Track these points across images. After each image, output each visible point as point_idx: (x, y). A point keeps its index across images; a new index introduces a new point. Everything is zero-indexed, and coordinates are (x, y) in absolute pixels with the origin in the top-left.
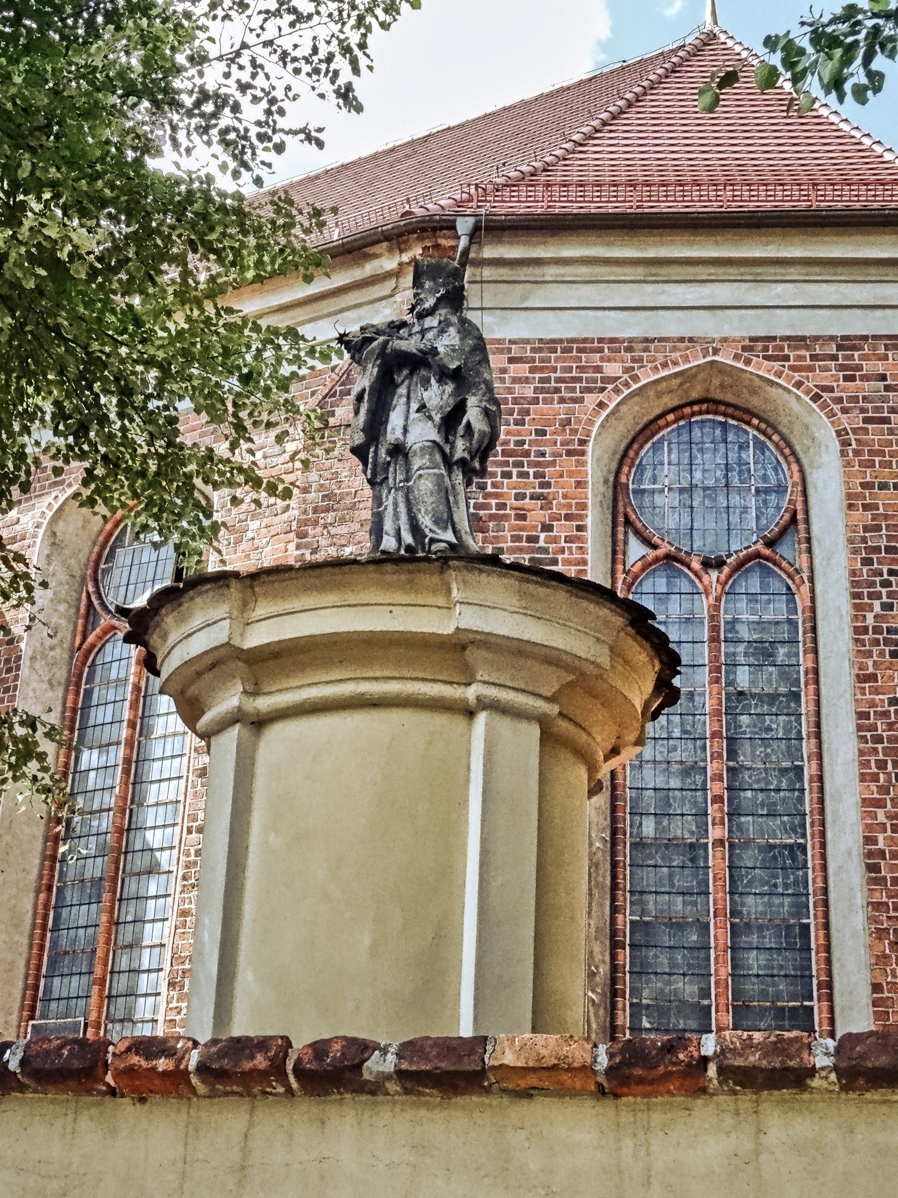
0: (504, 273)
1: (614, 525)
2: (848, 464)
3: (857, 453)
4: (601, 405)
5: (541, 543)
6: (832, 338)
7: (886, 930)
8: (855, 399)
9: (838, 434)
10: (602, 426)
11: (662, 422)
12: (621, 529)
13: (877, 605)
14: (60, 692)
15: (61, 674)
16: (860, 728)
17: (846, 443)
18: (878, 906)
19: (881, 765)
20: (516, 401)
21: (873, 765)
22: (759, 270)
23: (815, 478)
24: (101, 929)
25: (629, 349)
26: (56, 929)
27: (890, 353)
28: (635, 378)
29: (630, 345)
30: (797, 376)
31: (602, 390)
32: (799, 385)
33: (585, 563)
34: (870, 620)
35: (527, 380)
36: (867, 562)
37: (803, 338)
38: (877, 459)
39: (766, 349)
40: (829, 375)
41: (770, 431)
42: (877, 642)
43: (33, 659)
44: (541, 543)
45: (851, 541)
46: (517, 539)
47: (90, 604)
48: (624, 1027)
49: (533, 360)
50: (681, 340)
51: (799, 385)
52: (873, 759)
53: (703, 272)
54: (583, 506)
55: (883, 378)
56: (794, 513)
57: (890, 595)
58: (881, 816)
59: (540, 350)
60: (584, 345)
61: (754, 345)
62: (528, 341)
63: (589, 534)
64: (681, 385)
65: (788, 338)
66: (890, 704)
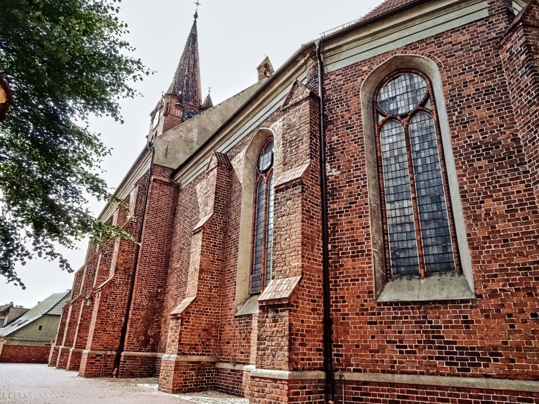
0: (332, 53)
1: (373, 113)
2: (442, 72)
3: (444, 68)
4: (363, 80)
5: (349, 123)
6: (432, 36)
7: (470, 216)
8: (442, 52)
9: (438, 64)
10: (364, 85)
11: (385, 80)
12: (375, 114)
13: (456, 113)
14: (252, 195)
15: (253, 190)
16: (454, 153)
17: (440, 67)
18: (466, 209)
19: (463, 163)
20: (338, 86)
21: (460, 164)
22: (405, 25)
23: (434, 81)
24: (263, 252)
25: (369, 62)
26: (256, 252)
27: (453, 35)
28: (372, 69)
29: (369, 60)
30: (422, 52)
31: (362, 75)
32: (422, 54)
33: (362, 125)
34: (454, 118)
35: (341, 80)
36: (451, 101)
37: (423, 40)
38: (452, 68)
39: (411, 47)
40: (433, 48)
41: (418, 72)
42: (458, 125)
43: (245, 188)
44: (349, 123)
45: (445, 96)
46: (342, 124)
47: (257, 173)
48: (389, 258)
49: (342, 74)
50: (384, 53)
51: (422, 54)
52: (460, 162)
53: (388, 32)
54: (360, 109)
55: (451, 42)
56: (429, 94)
57: (460, 109)
58: (465, 179)
59: (344, 70)
60: (356, 65)
61: (407, 47)
62: (340, 69)
63: (362, 117)
64: (387, 67)
65: (416, 42)
66: (464, 143)
